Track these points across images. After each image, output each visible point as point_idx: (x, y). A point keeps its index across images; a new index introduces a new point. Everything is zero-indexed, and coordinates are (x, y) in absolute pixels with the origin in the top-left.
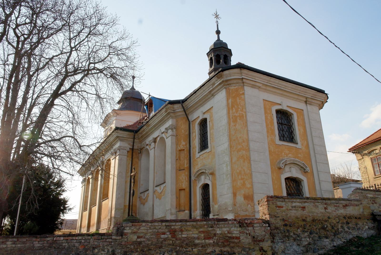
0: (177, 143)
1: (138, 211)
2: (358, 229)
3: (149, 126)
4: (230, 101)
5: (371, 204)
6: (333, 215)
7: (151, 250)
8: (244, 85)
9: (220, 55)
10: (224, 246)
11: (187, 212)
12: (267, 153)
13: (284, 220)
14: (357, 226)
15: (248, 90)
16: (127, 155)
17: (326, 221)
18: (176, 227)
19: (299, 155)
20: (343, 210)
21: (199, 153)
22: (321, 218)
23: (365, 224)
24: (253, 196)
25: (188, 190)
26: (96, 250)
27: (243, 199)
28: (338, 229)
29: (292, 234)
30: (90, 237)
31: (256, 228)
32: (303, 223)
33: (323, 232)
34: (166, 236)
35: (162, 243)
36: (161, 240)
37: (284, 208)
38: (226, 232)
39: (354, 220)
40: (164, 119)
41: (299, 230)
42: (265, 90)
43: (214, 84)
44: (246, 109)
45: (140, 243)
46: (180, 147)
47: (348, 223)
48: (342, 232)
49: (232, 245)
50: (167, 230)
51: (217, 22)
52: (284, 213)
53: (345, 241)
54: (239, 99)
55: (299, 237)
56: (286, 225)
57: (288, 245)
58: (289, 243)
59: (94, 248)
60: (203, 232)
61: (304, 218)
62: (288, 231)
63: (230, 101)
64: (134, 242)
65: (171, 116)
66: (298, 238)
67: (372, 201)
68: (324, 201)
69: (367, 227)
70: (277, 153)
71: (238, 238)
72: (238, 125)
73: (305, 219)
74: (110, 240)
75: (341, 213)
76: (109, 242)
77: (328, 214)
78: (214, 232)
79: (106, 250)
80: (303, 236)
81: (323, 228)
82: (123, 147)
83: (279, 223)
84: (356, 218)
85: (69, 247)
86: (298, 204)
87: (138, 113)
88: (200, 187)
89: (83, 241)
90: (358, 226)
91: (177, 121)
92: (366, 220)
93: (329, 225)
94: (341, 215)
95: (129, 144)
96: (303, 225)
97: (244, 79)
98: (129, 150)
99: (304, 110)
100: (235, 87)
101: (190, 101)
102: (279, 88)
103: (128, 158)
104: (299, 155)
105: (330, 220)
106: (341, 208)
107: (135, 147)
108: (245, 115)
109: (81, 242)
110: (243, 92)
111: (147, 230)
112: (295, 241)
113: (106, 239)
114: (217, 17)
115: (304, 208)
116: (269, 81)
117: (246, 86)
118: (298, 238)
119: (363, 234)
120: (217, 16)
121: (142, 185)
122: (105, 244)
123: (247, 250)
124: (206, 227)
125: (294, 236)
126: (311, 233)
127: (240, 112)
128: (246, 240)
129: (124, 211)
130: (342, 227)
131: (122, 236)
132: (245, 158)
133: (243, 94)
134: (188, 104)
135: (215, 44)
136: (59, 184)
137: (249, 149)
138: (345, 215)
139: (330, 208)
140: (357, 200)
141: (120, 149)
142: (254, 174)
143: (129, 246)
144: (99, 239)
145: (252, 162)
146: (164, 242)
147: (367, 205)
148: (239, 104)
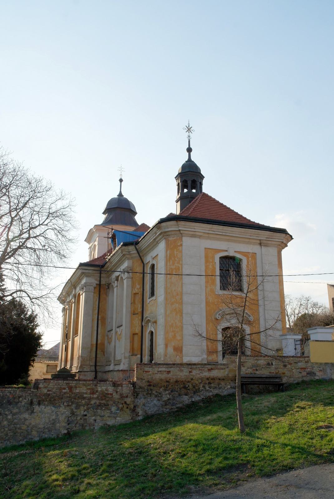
0: (133, 287)
1: (105, 350)
2: (220, 388)
3: (111, 263)
4: (168, 252)
6: (197, 377)
7: (55, 400)
8: (182, 236)
9: (190, 177)
10: (102, 400)
11: (139, 356)
12: (203, 305)
13: (148, 382)
14: (219, 386)
15: (187, 241)
16: (93, 291)
17: (189, 382)
18: (73, 385)
20: (207, 373)
21: (149, 298)
22: (184, 380)
23: (228, 384)
24: (182, 347)
25: (140, 334)
26: (21, 399)
27: (172, 350)
28: (199, 388)
29: (154, 392)
30: (16, 389)
31: (124, 388)
32: (165, 384)
33: (183, 391)
34: (66, 391)
35: (63, 395)
36: (62, 393)
37: (150, 373)
38: (105, 390)
39: (217, 381)
40: (121, 259)
41: (161, 389)
42: (209, 238)
43: (156, 233)
44: (182, 261)
45: (49, 395)
46: (134, 290)
47: (210, 383)
48: (202, 390)
49: (107, 399)
50: (66, 387)
51: (189, 136)
52: (149, 377)
53: (204, 397)
54: (177, 251)
55: (160, 394)
56: (150, 385)
57: (149, 400)
58: (150, 399)
59: (19, 397)
60: (90, 389)
61: (168, 380)
62: (151, 390)
63: (168, 252)
64: (45, 394)
65: (126, 257)
66: (160, 395)
68: (190, 366)
69: (229, 387)
71: (111, 394)
72: (173, 278)
73: (169, 381)
74: (30, 392)
75: (205, 376)
76: (29, 393)
77: (192, 377)
78: (97, 389)
79: (27, 399)
80: (164, 393)
81: (185, 387)
82: (89, 283)
83: (144, 384)
84: (219, 379)
85: (3, 396)
86: (164, 369)
87: (124, 228)
88: (148, 333)
89: (12, 392)
90: (220, 386)
91: (133, 262)
92: (230, 381)
93: (190, 385)
94: (205, 377)
95: (96, 280)
96: (165, 386)
97: (181, 231)
98: (95, 286)
99: (257, 254)
100: (174, 239)
101: (143, 243)
102: (224, 234)
103: (95, 295)
105: (192, 381)
106: (206, 371)
107: (103, 283)
108: (181, 268)
109: (11, 393)
110: (181, 243)
111: (54, 386)
112: (156, 397)
113: (27, 391)
114: (189, 130)
117: (185, 236)
118: (160, 395)
119: (224, 392)
120: (189, 129)
121: (110, 322)
122: (27, 394)
123: (117, 403)
124: (92, 385)
125: (156, 394)
126: (172, 391)
127: (177, 265)
128: (116, 396)
129: (91, 350)
130: (203, 386)
131: (37, 389)
132: (178, 311)
133: (181, 245)
134: (141, 246)
135: (184, 167)
136: (32, 319)
137: (182, 302)
138: (208, 377)
139: (195, 372)
140: (224, 365)
141: (86, 285)
142: (184, 327)
143: (41, 397)
144: (22, 391)
145: (184, 315)
146: (64, 395)
148: (176, 255)
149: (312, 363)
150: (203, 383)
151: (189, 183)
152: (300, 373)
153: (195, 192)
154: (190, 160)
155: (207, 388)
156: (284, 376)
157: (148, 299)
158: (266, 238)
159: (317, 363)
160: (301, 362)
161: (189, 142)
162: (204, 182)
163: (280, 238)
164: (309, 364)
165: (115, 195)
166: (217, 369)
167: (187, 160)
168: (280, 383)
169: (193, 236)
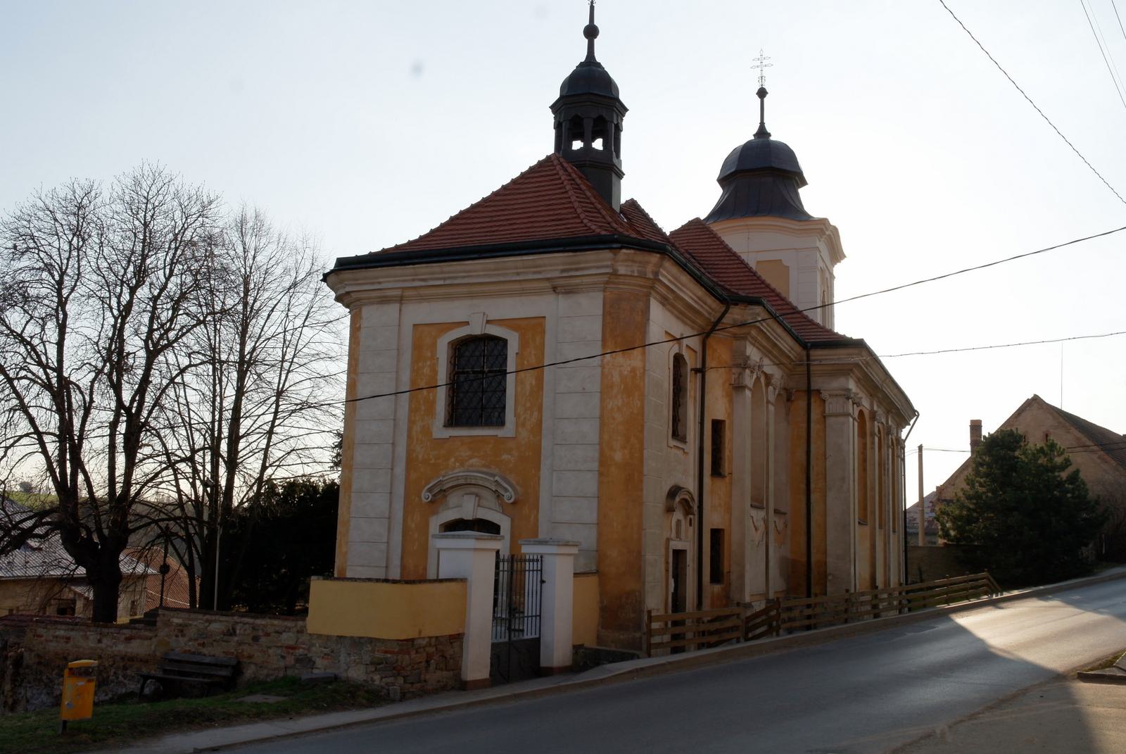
5: (174, 638)
13: (39, 656)
19: (505, 457)
29: (44, 677)
37: (43, 639)
47: (125, 668)
48: (112, 682)
56: (40, 663)
67: (176, 631)
70: (432, 461)
75: (119, 651)
86: (62, 633)
102: (448, 282)
104: (505, 457)
115: (68, 639)
116: (417, 275)
147: (166, 638)
149: (310, 634)
150: (115, 666)
151: (588, 126)
152: (283, 657)
153: (601, 148)
155: (121, 678)
156: (249, 663)
158: (563, 271)
159: (320, 636)
160: (289, 632)
161: (592, 8)
162: (627, 122)
163: (600, 264)
164: (304, 638)
165: (746, 135)
166: (140, 638)
167: (583, 60)
169: (384, 300)
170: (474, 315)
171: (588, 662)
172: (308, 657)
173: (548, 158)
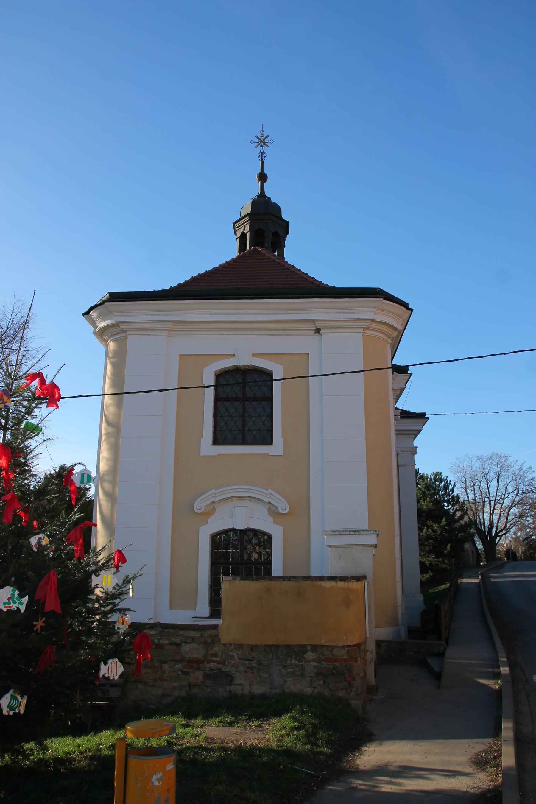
51: (262, 153)
149: (225, 645)
154: (262, 195)
157: (370, 577)
159: (240, 646)
168: (378, 789)
170: (244, 352)
171: (392, 654)
172: (223, 672)
173: (233, 260)
